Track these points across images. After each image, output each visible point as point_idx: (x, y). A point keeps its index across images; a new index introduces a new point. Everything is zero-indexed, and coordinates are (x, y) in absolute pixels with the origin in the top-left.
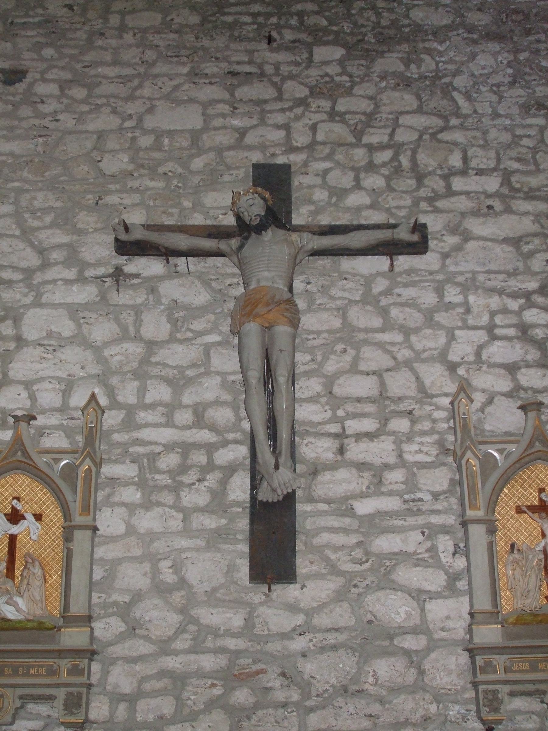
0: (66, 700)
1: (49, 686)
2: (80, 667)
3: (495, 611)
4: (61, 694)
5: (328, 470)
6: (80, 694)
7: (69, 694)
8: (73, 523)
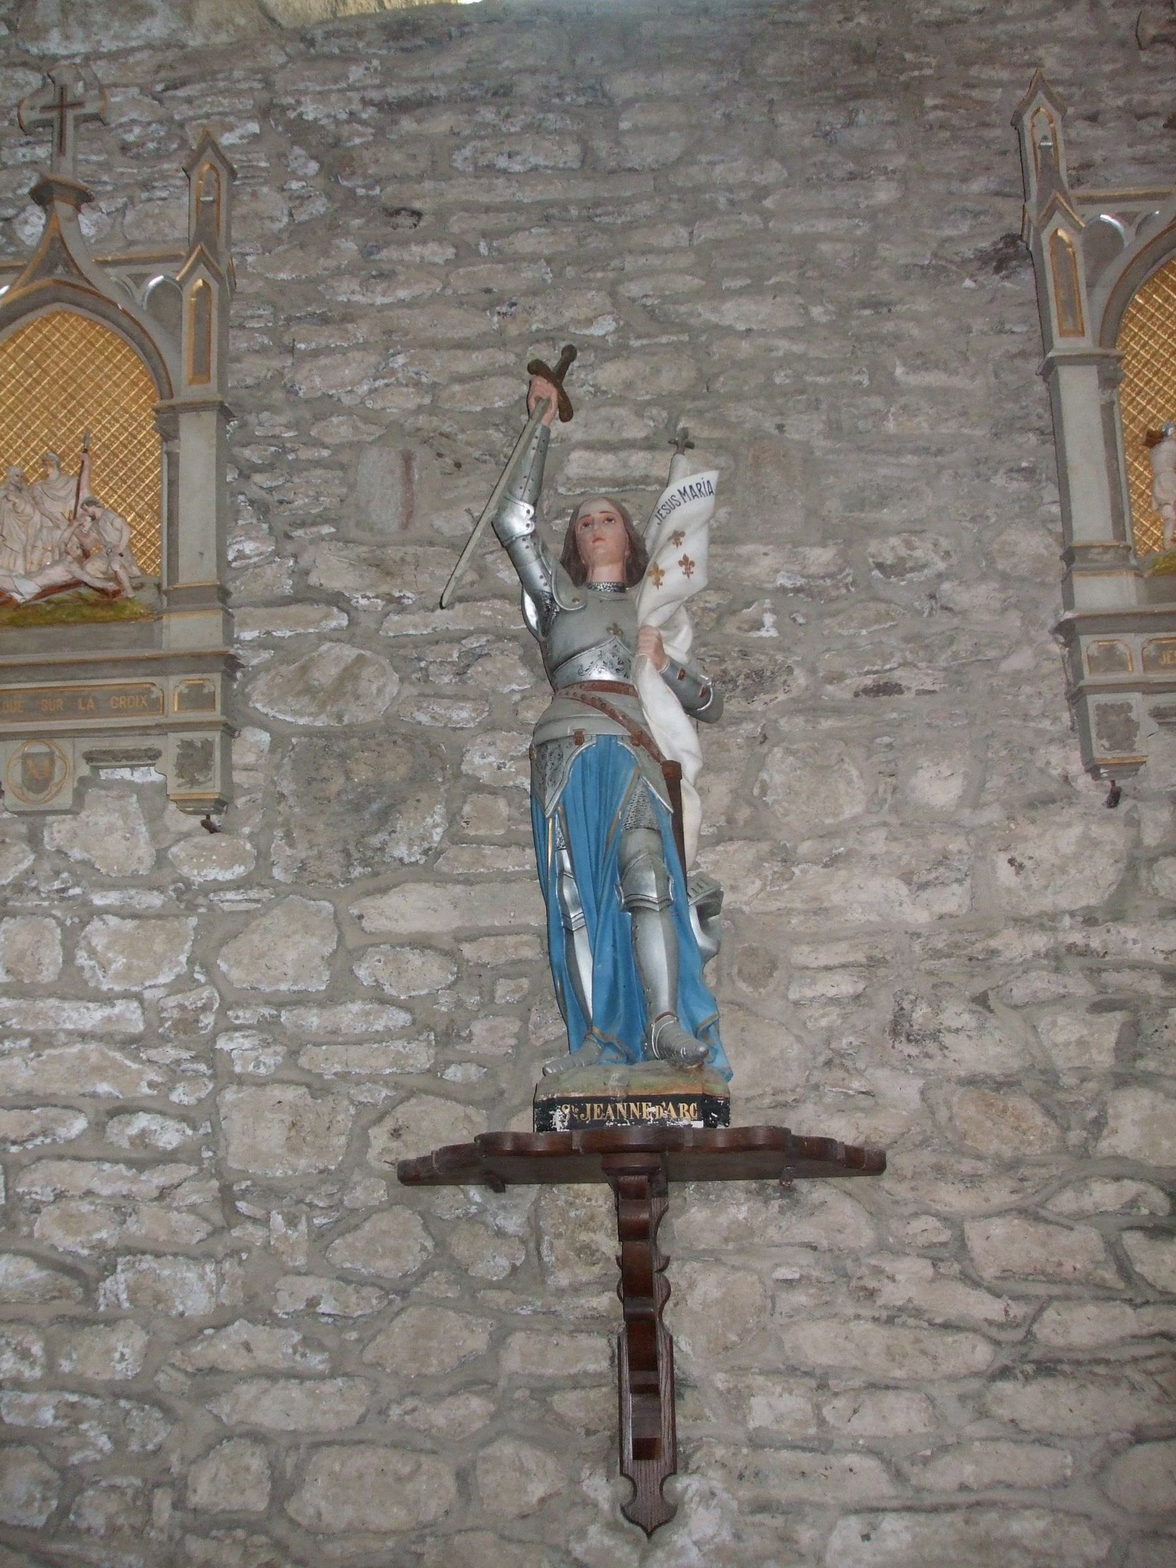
0: (181, 756)
1: (144, 730)
2: (206, 691)
3: (1122, 544)
4: (170, 745)
5: (1122, 884)
6: (208, 745)
7: (188, 745)
8: (175, 401)
